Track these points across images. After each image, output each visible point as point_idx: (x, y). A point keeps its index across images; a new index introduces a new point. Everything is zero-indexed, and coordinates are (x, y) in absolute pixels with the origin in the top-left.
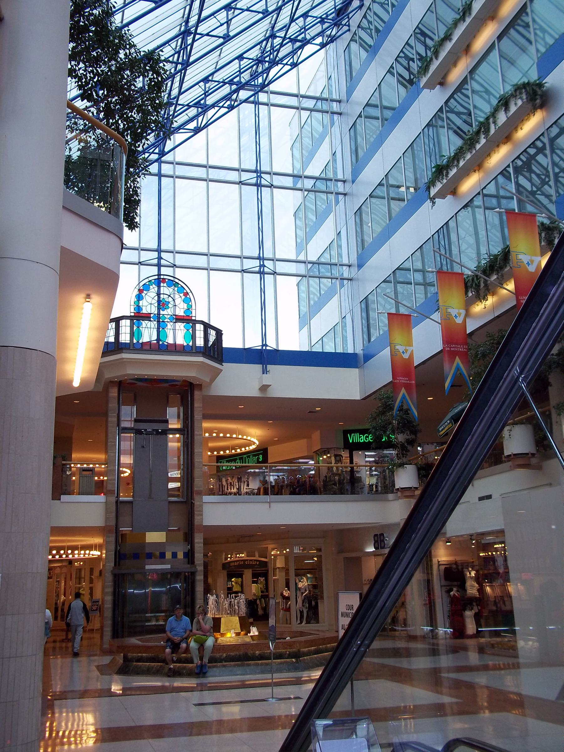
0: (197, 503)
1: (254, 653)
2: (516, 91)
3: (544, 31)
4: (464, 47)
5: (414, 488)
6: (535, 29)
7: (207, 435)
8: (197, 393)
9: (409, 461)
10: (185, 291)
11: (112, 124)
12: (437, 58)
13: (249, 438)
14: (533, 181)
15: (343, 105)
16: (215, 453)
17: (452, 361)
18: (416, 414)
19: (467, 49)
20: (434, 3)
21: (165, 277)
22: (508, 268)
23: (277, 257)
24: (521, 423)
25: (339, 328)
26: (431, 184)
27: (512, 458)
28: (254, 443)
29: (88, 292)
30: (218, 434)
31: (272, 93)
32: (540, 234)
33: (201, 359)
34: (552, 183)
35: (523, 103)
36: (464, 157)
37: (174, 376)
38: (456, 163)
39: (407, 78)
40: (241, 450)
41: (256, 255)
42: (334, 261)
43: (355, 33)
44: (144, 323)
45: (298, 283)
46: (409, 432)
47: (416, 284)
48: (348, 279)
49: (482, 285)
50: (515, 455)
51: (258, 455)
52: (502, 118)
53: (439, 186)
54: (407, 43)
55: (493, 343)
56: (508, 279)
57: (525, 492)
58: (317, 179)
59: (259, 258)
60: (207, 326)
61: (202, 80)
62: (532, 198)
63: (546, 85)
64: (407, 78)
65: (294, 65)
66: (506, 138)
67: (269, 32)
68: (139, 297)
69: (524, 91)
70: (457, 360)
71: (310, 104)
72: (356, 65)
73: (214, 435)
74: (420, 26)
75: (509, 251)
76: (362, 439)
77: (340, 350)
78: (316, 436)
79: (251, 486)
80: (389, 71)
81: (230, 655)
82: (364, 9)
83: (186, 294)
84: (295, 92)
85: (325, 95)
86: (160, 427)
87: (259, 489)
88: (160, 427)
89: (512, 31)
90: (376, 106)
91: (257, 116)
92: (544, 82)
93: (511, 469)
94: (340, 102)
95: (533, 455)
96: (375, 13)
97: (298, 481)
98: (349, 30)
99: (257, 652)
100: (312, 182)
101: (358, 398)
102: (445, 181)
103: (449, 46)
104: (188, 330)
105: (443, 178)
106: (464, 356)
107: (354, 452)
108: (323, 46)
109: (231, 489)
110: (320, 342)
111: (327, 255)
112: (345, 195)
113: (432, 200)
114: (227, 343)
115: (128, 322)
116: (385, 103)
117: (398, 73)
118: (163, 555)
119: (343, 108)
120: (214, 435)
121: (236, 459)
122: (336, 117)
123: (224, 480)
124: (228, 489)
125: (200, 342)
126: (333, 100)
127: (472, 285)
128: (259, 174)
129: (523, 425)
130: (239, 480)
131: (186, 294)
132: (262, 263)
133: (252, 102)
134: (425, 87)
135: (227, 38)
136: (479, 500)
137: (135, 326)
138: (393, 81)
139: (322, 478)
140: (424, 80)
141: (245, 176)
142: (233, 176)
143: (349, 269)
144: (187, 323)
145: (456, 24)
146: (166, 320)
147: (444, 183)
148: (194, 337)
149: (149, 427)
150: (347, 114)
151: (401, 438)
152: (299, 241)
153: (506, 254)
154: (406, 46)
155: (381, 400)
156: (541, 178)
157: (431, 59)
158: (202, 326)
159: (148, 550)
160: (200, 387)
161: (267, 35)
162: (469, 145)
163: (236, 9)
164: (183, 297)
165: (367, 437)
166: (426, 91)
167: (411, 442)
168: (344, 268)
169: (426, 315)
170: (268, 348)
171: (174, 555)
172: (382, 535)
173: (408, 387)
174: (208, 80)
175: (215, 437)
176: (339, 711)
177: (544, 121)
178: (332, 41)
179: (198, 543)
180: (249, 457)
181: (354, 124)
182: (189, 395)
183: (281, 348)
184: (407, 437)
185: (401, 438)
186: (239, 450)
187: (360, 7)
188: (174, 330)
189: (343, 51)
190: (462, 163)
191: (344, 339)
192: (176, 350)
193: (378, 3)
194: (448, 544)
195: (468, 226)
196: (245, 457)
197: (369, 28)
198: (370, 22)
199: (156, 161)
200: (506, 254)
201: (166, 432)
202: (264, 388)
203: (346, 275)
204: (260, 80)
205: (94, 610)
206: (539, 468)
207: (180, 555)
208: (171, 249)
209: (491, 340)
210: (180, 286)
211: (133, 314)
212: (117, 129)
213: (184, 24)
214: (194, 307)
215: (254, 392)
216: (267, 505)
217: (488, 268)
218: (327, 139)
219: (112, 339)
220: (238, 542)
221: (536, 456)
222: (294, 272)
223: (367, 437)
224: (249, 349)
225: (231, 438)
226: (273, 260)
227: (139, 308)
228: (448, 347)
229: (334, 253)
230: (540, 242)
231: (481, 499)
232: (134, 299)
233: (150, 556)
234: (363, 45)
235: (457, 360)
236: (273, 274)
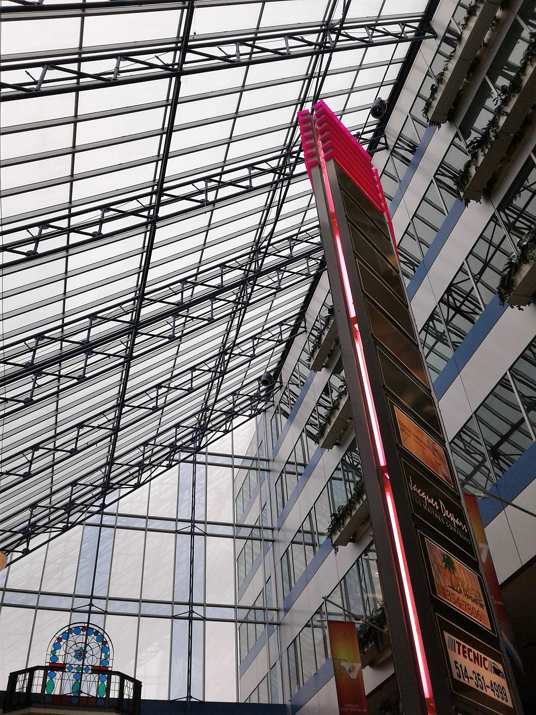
12: (330, 424)
23: (208, 602)
68: (57, 646)
82: (283, 389)
90: (293, 463)
96: (290, 390)
98: (273, 405)
102: (342, 529)
108: (251, 417)
115: (42, 672)
125: (114, 694)
126: (262, 460)
137: (48, 677)
142: (171, 526)
148: (108, 690)
163: (239, 394)
170: (192, 700)
187: (281, 387)
190: (353, 513)
199: (97, 512)
208: (202, 602)
211: (48, 664)
214: (111, 657)
232: (51, 648)
234: (286, 415)
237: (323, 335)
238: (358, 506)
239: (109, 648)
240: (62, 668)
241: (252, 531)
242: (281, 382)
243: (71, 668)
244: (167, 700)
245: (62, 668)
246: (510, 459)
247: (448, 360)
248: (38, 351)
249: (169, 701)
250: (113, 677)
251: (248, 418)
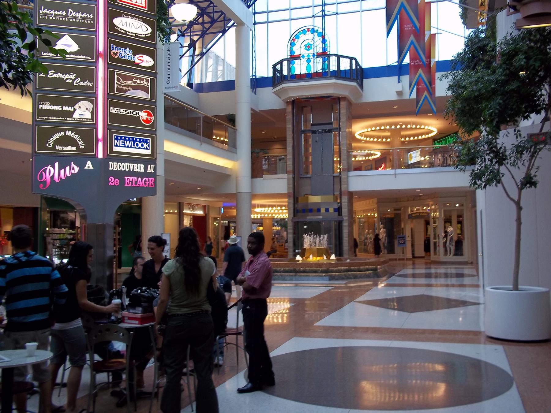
1: (299, 269)
10: (306, 30)
13: (426, 127)
30: (401, 126)
33: (333, 81)
37: (321, 94)
44: (297, 61)
68: (292, 44)
81: (285, 269)
86: (327, 128)
88: (327, 128)
99: (302, 268)
118: (319, 210)
149: (320, 128)
159: (309, 208)
171: (327, 210)
176: (434, 310)
179: (344, 202)
183: (440, 60)
205: (401, 244)
207: (331, 210)
214: (328, 45)
215: (393, 97)
219: (335, 69)
220: (414, 200)
225: (420, 128)
227: (291, 51)
233: (311, 211)
235: (420, 71)
239: (303, 30)
240: (298, 57)
243: (303, 57)
245: (298, 57)
249: (387, 66)
250: (331, 58)
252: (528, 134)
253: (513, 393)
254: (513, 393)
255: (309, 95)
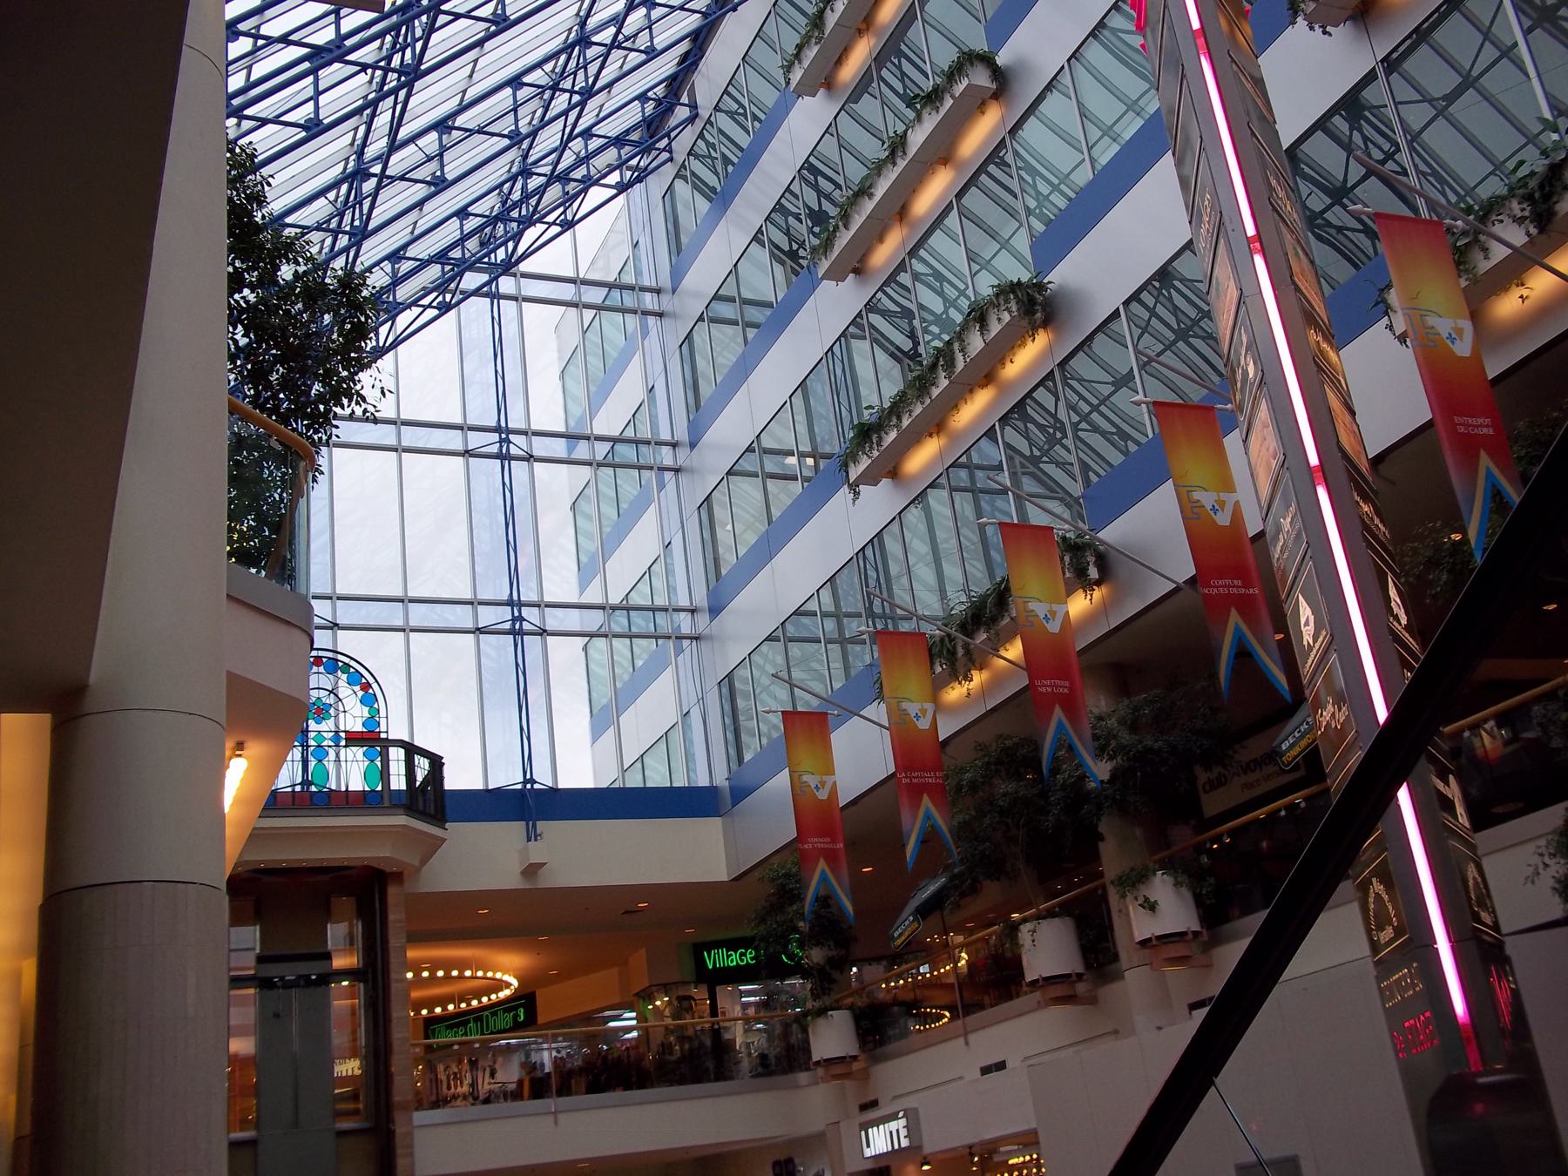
0: (400, 1129)
2: (997, 295)
3: (1033, 172)
4: (898, 209)
5: (851, 1057)
6: (1018, 168)
7: (410, 975)
8: (392, 891)
9: (837, 1001)
10: (364, 681)
11: (267, 400)
12: (846, 227)
13: (499, 975)
14: (1031, 435)
15: (665, 298)
16: (424, 1012)
17: (916, 805)
18: (849, 907)
19: (902, 213)
20: (833, 125)
21: (321, 653)
22: (1006, 620)
23: (547, 599)
24: (1050, 914)
25: (677, 736)
26: (849, 459)
27: (1042, 986)
28: (508, 985)
29: (240, 738)
31: (524, 275)
32: (1062, 559)
33: (402, 820)
34: (1069, 442)
35: (1013, 317)
36: (911, 411)
38: (894, 420)
39: (787, 248)
40: (480, 1002)
41: (505, 597)
42: (660, 601)
43: (683, 166)
45: (586, 645)
46: (832, 944)
47: (829, 641)
48: (691, 638)
49: (960, 652)
50: (1159, 938)
51: (516, 1008)
52: (976, 343)
53: (864, 463)
54: (788, 189)
55: (988, 763)
56: (1009, 639)
57: (1071, 1050)
58: (615, 440)
59: (510, 603)
60: (411, 750)
61: (387, 258)
62: (1032, 469)
63: (1049, 286)
64: (787, 248)
65: (568, 225)
66: (985, 377)
67: (516, 163)
69: (1012, 297)
70: (926, 800)
71: (595, 295)
72: (687, 222)
73: (425, 974)
74: (812, 159)
75: (1007, 589)
76: (732, 961)
77: (680, 782)
78: (639, 959)
79: (500, 1077)
80: (755, 239)
82: (699, 124)
83: (366, 687)
84: (571, 274)
85: (629, 279)
86: (313, 970)
87: (520, 1083)
88: (313, 970)
89: (983, 178)
90: (731, 300)
91: (496, 321)
92: (1045, 281)
93: (1040, 1006)
94: (658, 291)
95: (1079, 976)
96: (721, 131)
97: (605, 1058)
98: (671, 159)
100: (607, 446)
101: (723, 876)
102: (876, 453)
103: (868, 206)
104: (372, 761)
105: (871, 448)
106: (936, 792)
107: (718, 988)
108: (622, 188)
109: (456, 1089)
110: (639, 765)
111: (644, 587)
112: (677, 471)
113: (854, 488)
114: (454, 780)
116: (746, 294)
117: (770, 241)
119: (666, 303)
120: (425, 974)
121: (468, 1022)
122: (651, 320)
123: (441, 1068)
124: (449, 1088)
125: (398, 782)
126: (644, 289)
127: (941, 651)
128: (503, 436)
129: (1056, 919)
130: (473, 1064)
131: (366, 687)
132: (516, 614)
133: (486, 295)
134: (826, 276)
135: (440, 184)
136: (982, 1075)
138: (762, 254)
139: (654, 1046)
140: (824, 265)
141: (475, 440)
142: (454, 440)
143: (693, 618)
144: (371, 747)
145: (878, 168)
146: (325, 743)
147: (875, 456)
148: (385, 774)
149: (290, 972)
150: (673, 315)
151: (817, 955)
152: (584, 559)
153: (1001, 595)
154: (787, 194)
155: (773, 880)
156: (1048, 433)
157: (836, 228)
158: (402, 751)
160: (398, 877)
161: (514, 170)
162: (919, 389)
164: (361, 693)
165: (742, 955)
166: (828, 285)
167: (841, 964)
168: (682, 615)
169: (852, 709)
170: (536, 786)
172: (790, 1161)
173: (831, 857)
174: (398, 258)
175: (426, 978)
177: (1050, 349)
178: (639, 180)
180: (494, 1014)
181: (689, 336)
182: (377, 896)
184: (831, 954)
185: (817, 955)
186: (475, 1003)
187: (691, 120)
188: (338, 760)
189: (660, 197)
190: (906, 422)
191: (689, 757)
192: (347, 804)
193: (726, 112)
194: (926, 1168)
195: (914, 521)
196: (487, 1016)
197: (710, 156)
198: (709, 145)
200: (1001, 595)
201: (327, 978)
202: (531, 870)
203: (686, 629)
204: (501, 254)
206: (1092, 1001)
208: (328, 591)
209: (985, 756)
210: (352, 670)
212: (275, 410)
213: (354, 157)
214: (383, 713)
216: (551, 1118)
217: (969, 620)
218: (637, 358)
221: (1085, 977)
222: (577, 628)
223: (742, 955)
224: (498, 791)
226: (539, 606)
228: (906, 777)
229: (659, 584)
230: (1064, 574)
231: (986, 1070)
234: (699, 185)
235: (926, 800)
236: (541, 634)
237: (828, 11)
238: (918, 409)
239: (375, 695)
241: (612, 447)
242: (693, 106)
244: (481, 788)
246: (1193, 288)
247: (1336, 285)
248: (447, 157)
251: (614, 191)
252: (1123, 978)
253: (1029, 978)
254: (1029, 978)
255: (304, 861)
